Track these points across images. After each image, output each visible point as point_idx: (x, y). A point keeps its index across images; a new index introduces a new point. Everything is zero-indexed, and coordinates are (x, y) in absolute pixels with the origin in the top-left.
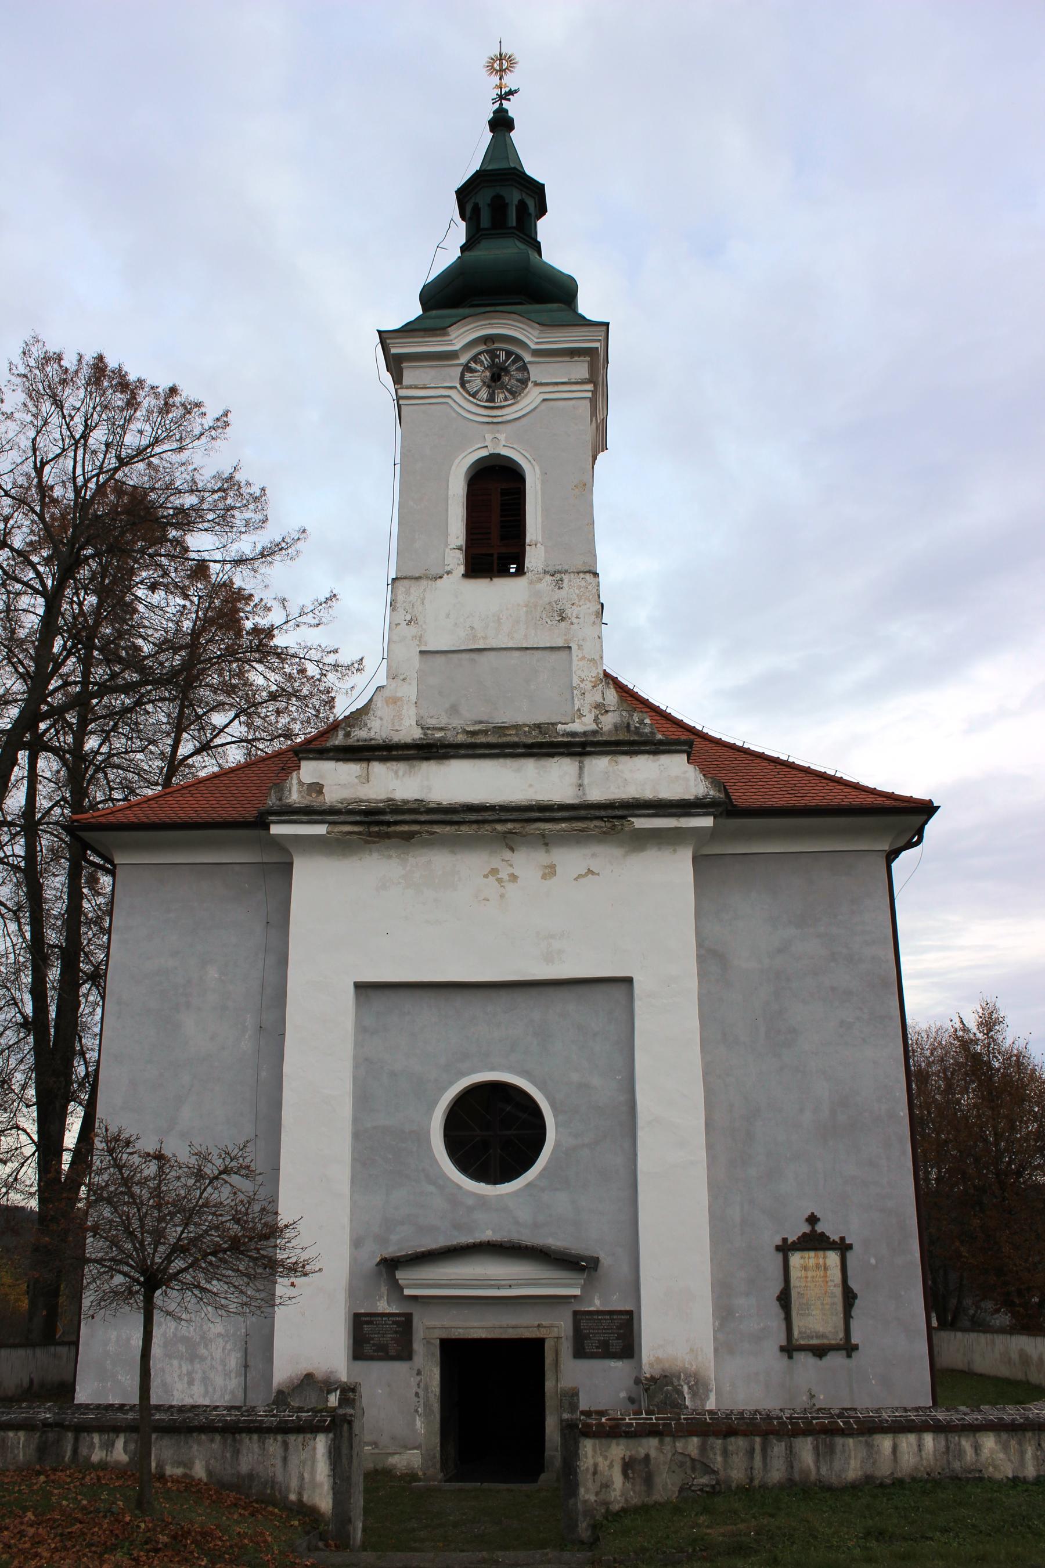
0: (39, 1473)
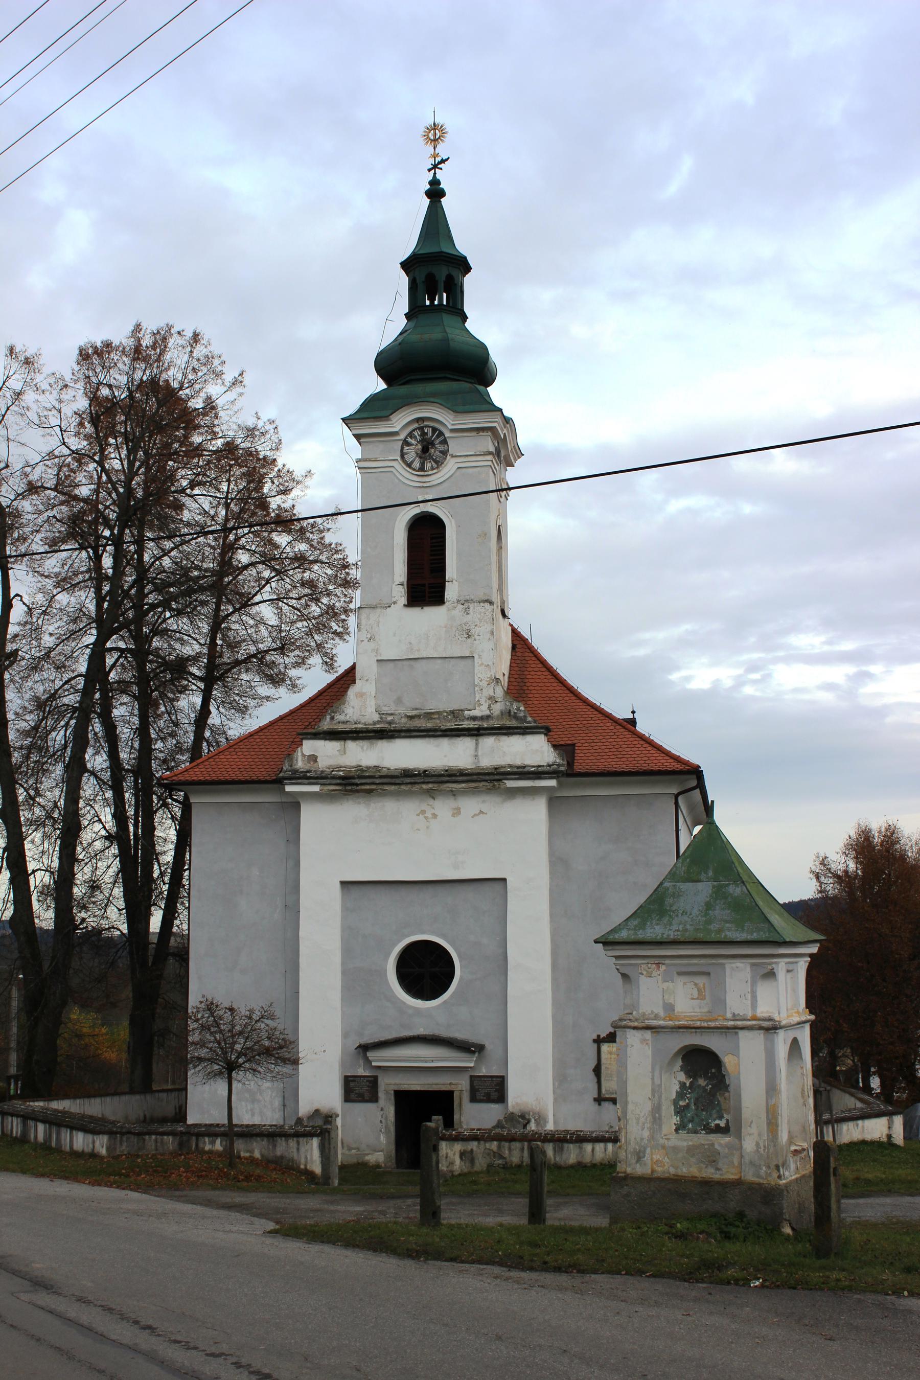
0: (181, 1155)
